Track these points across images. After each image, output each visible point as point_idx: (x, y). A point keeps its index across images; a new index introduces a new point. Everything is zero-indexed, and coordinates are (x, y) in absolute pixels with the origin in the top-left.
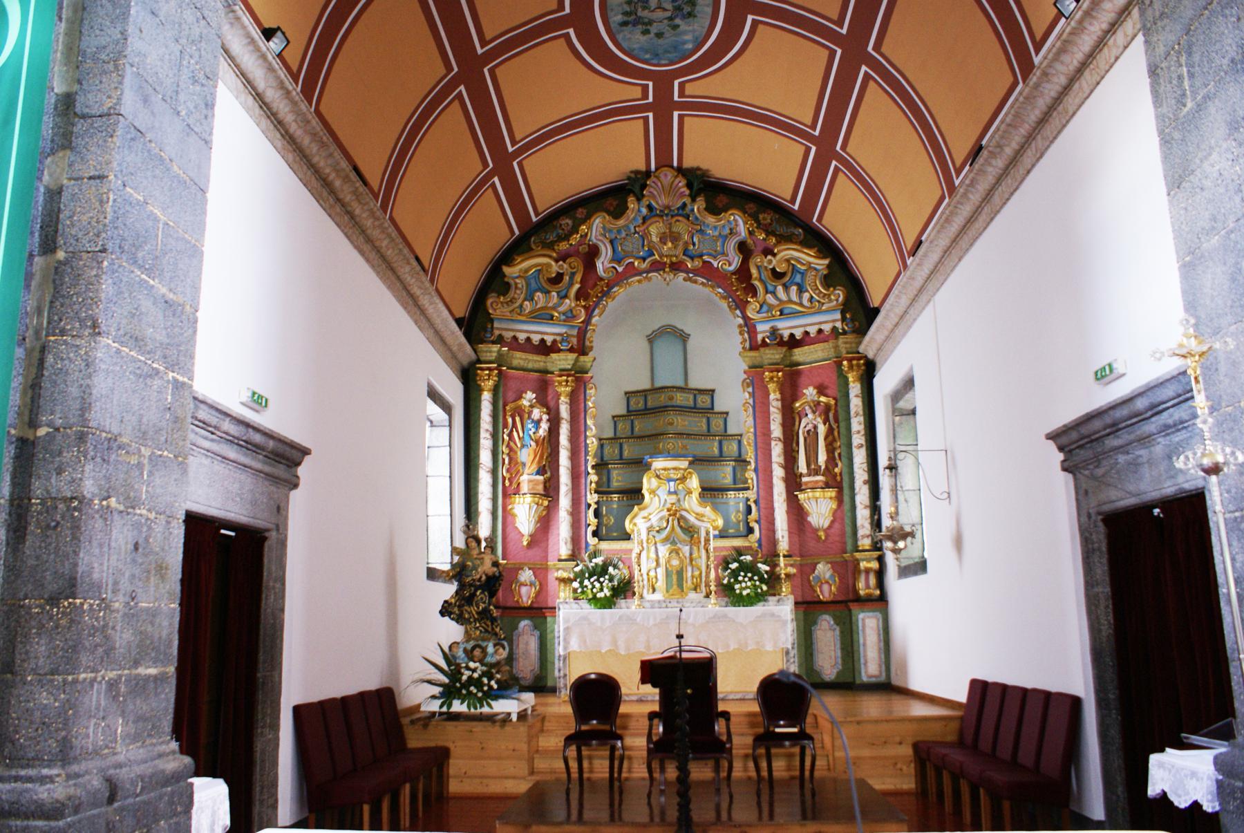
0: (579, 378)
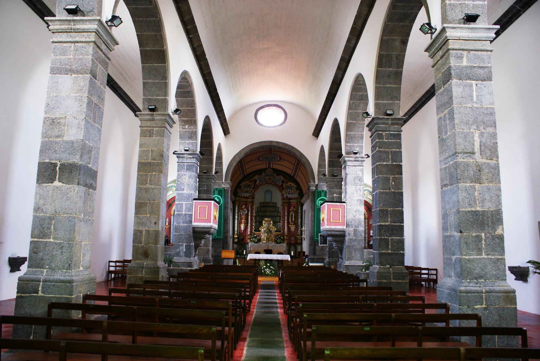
0: (252, 203)
